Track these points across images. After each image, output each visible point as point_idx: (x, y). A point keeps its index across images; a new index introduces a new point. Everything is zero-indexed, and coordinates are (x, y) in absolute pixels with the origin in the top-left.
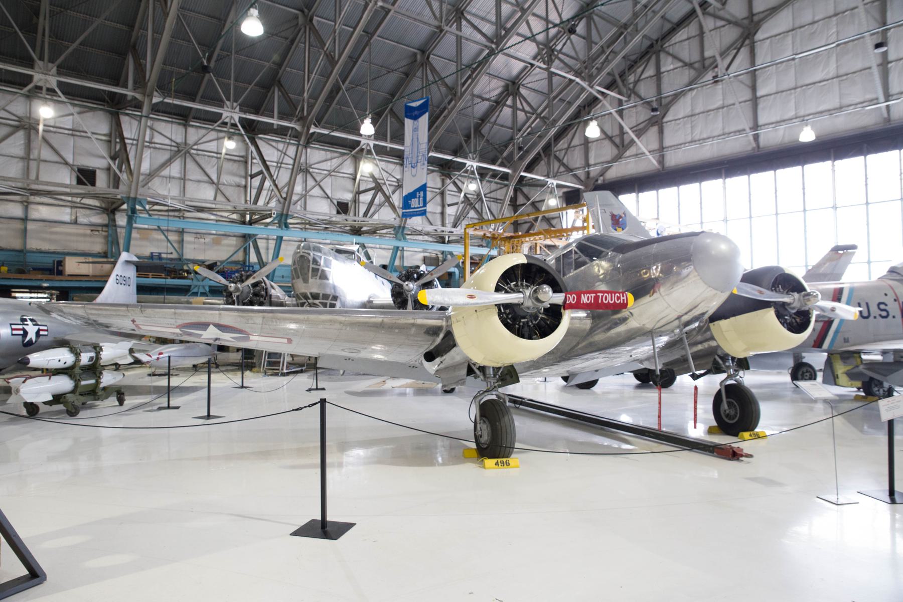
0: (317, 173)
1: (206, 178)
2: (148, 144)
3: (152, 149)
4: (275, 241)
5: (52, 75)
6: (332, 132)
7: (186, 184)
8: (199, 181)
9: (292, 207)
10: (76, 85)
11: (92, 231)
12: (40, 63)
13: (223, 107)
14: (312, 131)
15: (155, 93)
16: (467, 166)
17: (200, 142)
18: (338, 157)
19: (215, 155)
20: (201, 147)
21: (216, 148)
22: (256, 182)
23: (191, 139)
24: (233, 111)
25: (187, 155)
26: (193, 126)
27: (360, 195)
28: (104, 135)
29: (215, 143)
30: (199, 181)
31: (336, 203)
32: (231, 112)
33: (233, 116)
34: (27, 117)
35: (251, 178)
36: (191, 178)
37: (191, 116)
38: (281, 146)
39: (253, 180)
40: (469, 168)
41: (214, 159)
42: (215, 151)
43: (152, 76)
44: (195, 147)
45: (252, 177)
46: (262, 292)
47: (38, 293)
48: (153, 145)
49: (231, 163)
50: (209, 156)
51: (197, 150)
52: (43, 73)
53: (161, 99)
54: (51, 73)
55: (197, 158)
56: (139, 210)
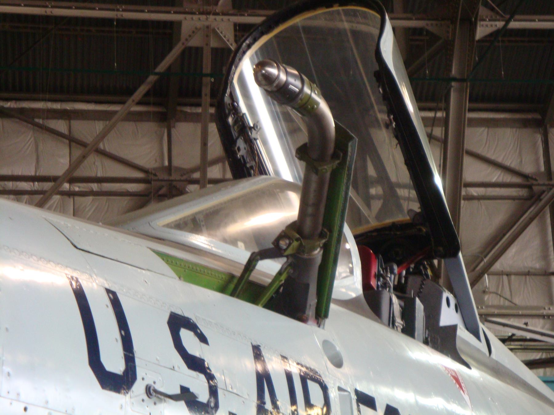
5: (224, 14)
15: (482, 11)
24: (209, 8)
33: (214, 25)
34: (163, 169)
38: (267, 74)
46: (107, 235)
53: (500, 24)
54: (218, 9)
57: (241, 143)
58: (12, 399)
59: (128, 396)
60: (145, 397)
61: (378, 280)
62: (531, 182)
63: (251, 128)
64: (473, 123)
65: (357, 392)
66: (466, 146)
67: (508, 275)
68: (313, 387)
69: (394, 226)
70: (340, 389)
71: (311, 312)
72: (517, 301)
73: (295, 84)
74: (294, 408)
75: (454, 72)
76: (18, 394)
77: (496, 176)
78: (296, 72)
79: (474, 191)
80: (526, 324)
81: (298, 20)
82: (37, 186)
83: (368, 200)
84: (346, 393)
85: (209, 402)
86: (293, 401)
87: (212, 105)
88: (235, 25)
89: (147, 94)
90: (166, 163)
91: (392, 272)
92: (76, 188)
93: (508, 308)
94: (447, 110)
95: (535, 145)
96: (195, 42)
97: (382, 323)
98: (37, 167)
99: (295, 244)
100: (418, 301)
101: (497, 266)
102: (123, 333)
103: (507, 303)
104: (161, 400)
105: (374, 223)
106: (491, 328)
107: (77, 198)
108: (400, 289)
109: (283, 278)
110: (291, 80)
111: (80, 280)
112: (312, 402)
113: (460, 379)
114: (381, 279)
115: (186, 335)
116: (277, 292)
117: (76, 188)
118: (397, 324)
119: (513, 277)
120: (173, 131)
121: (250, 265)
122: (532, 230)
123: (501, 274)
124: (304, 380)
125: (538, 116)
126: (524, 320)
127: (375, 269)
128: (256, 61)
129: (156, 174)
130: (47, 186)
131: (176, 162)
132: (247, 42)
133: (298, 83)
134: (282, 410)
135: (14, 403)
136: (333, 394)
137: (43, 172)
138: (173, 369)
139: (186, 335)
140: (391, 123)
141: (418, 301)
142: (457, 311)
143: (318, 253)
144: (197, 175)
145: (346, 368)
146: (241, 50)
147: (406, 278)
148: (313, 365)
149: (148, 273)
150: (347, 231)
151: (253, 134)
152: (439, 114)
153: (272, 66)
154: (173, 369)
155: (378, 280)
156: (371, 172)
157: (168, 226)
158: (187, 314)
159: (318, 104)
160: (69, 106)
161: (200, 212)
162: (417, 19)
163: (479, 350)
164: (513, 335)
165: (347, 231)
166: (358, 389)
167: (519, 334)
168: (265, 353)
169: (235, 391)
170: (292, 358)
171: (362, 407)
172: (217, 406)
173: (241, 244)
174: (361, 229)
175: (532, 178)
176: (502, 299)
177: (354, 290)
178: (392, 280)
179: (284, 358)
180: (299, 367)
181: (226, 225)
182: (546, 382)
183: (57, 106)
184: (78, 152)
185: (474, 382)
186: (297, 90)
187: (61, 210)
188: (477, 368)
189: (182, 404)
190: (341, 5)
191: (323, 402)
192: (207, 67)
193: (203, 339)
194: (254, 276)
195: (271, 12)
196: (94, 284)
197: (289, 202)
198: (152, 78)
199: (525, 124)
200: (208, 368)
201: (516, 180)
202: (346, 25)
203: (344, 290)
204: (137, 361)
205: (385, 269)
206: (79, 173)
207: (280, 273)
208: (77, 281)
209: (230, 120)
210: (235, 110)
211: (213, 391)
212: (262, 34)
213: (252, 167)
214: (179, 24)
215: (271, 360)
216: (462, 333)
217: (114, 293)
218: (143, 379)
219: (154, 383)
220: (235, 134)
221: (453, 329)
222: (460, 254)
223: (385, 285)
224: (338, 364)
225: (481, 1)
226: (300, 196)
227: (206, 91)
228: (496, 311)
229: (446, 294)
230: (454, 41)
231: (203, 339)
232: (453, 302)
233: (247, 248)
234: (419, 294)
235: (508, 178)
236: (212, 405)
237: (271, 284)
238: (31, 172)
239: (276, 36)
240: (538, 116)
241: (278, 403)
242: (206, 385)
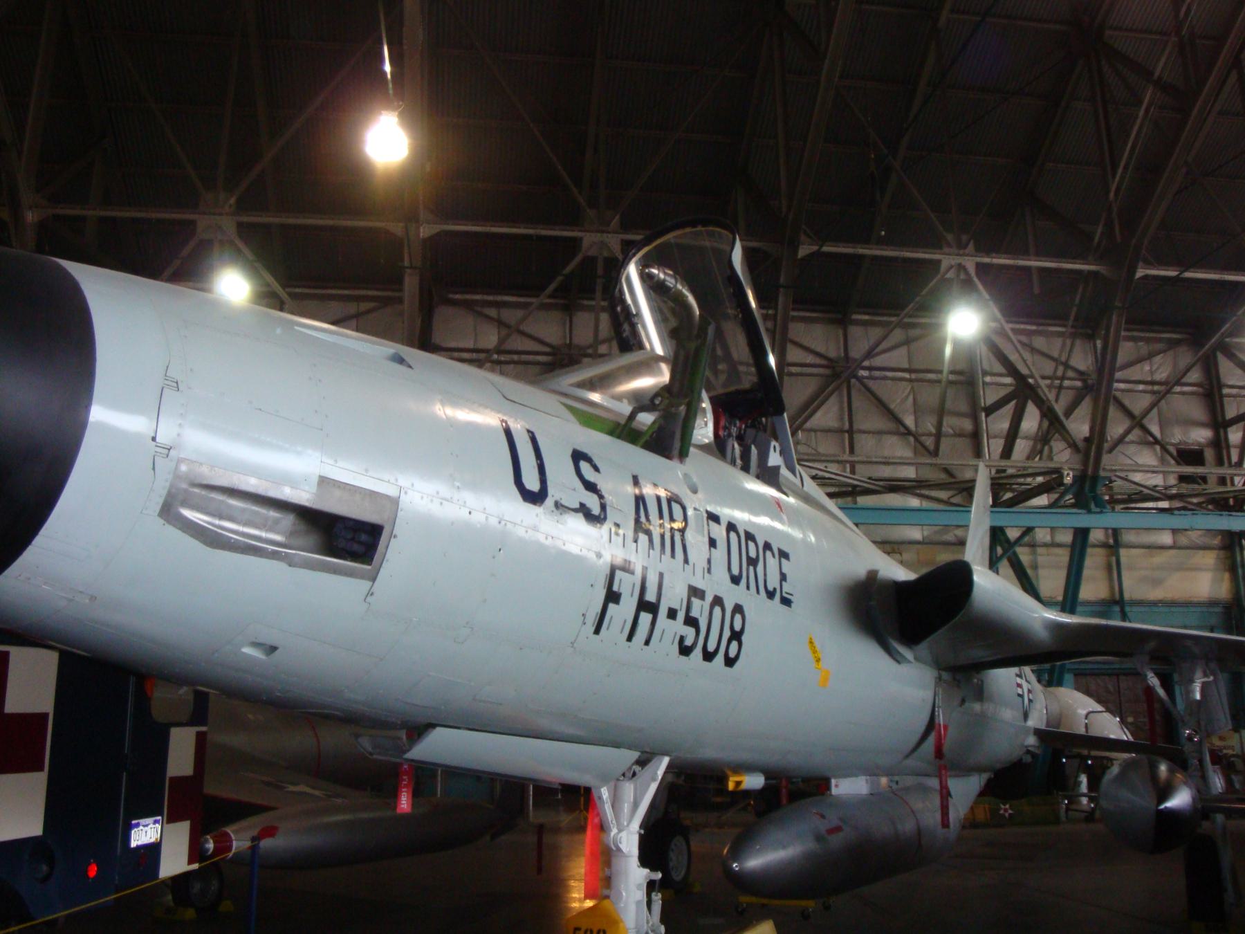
0: (1123, 391)
1: (891, 425)
4: (1069, 549)
6: (1185, 271)
7: (855, 440)
8: (880, 433)
9: (1106, 460)
12: (591, 213)
13: (940, 248)
14: (1140, 273)
15: (803, 237)
17: (878, 350)
18: (1165, 351)
19: (907, 375)
20: (878, 361)
21: (906, 360)
22: (1000, 423)
23: (858, 348)
24: (961, 252)
25: (853, 381)
27: (1229, 430)
29: (903, 351)
30: (880, 433)
31: (1175, 453)
32: (957, 255)
35: (987, 416)
36: (863, 427)
39: (990, 419)
41: (904, 383)
42: (906, 366)
44: (866, 363)
45: (990, 411)
47: (367, 289)
50: (893, 379)
51: (870, 369)
52: (598, 231)
53: (815, 248)
55: (870, 383)
56: (1095, 346)
57: (626, 327)
58: (461, 505)
59: (542, 508)
60: (554, 509)
61: (725, 431)
63: (634, 315)
64: (795, 319)
65: (707, 512)
66: (789, 336)
67: (815, 431)
68: (675, 507)
69: (738, 392)
70: (695, 509)
71: (676, 452)
72: (821, 450)
73: (670, 282)
74: (662, 521)
75: (782, 280)
76: (465, 502)
77: (810, 359)
78: (671, 272)
79: (794, 369)
80: (826, 467)
81: (669, 237)
82: (474, 356)
83: (716, 372)
84: (699, 512)
85: (600, 515)
86: (661, 517)
87: (604, 300)
88: (622, 240)
89: (556, 290)
90: (568, 342)
91: (735, 426)
92: (502, 358)
93: (813, 455)
94: (776, 308)
96: (591, 253)
97: (726, 462)
98: (476, 341)
99: (666, 402)
100: (753, 447)
101: (808, 425)
102: (539, 462)
103: (813, 452)
104: (565, 512)
105: (721, 391)
106: (515, 524)
107: (502, 366)
108: (740, 438)
109: (656, 426)
110: (668, 278)
111: (509, 423)
112: (675, 517)
113: (781, 504)
114: (727, 430)
115: (584, 466)
116: (651, 436)
117: (502, 358)
118: (737, 464)
119: (819, 433)
120: (575, 320)
121: (632, 416)
122: (833, 400)
123: (810, 430)
124: (669, 501)
125: (840, 316)
126: (825, 464)
127: (723, 423)
128: (643, 264)
130: (482, 356)
131: (576, 341)
132: (633, 251)
133: (673, 281)
134: (653, 522)
135: (462, 507)
136: (690, 512)
137: (481, 345)
138: (574, 490)
139: (584, 466)
140: (738, 315)
141: (753, 447)
142: (781, 455)
143: (682, 408)
144: (590, 351)
145: (700, 495)
146: (629, 257)
147: (745, 430)
148: (676, 491)
149: (557, 419)
150: (704, 395)
151: (635, 320)
152: (770, 312)
153: (653, 268)
154: (574, 490)
155: (725, 431)
156: (719, 352)
157: (572, 385)
158: (585, 450)
159: (687, 297)
160: (499, 298)
161: (595, 376)
163: (795, 484)
164: (817, 475)
165: (704, 395)
166: (709, 509)
167: (821, 474)
168: (641, 481)
169: (619, 508)
170: (1082, 389)
171: (711, 522)
172: (605, 519)
173: (625, 401)
174: (713, 393)
176: (810, 449)
177: (707, 437)
178: (734, 431)
179: (655, 485)
180: (666, 492)
181: (615, 386)
182: (840, 508)
183: (490, 298)
184: (504, 332)
185: (790, 506)
186: (672, 286)
187: (493, 370)
188: (794, 497)
189: (580, 515)
190: (703, 226)
191: (682, 518)
192: (600, 271)
193: (596, 469)
194: (634, 425)
195: (648, 232)
196: (519, 426)
197: (660, 373)
198: (560, 278)
199: (832, 322)
200: (600, 490)
201: (823, 362)
202: (707, 244)
203: (700, 437)
204: (549, 483)
205: (730, 424)
206: (503, 348)
207: (654, 422)
208: (506, 422)
209: (619, 309)
210: (623, 301)
211: (603, 507)
212: (645, 245)
213: (634, 345)
214: (581, 239)
215: (646, 486)
216: (784, 472)
217: (532, 433)
218: (553, 496)
219: (561, 499)
220: (622, 319)
221: (777, 468)
222: (785, 415)
223: (730, 435)
224: (695, 491)
226: (670, 367)
227: (599, 288)
228: (806, 457)
229: (773, 443)
231: (596, 469)
232: (778, 449)
233: (630, 403)
234: (754, 442)
235: (818, 361)
236: (602, 517)
237: (647, 430)
238: (471, 346)
239: (655, 247)
241: (650, 518)
242: (599, 503)
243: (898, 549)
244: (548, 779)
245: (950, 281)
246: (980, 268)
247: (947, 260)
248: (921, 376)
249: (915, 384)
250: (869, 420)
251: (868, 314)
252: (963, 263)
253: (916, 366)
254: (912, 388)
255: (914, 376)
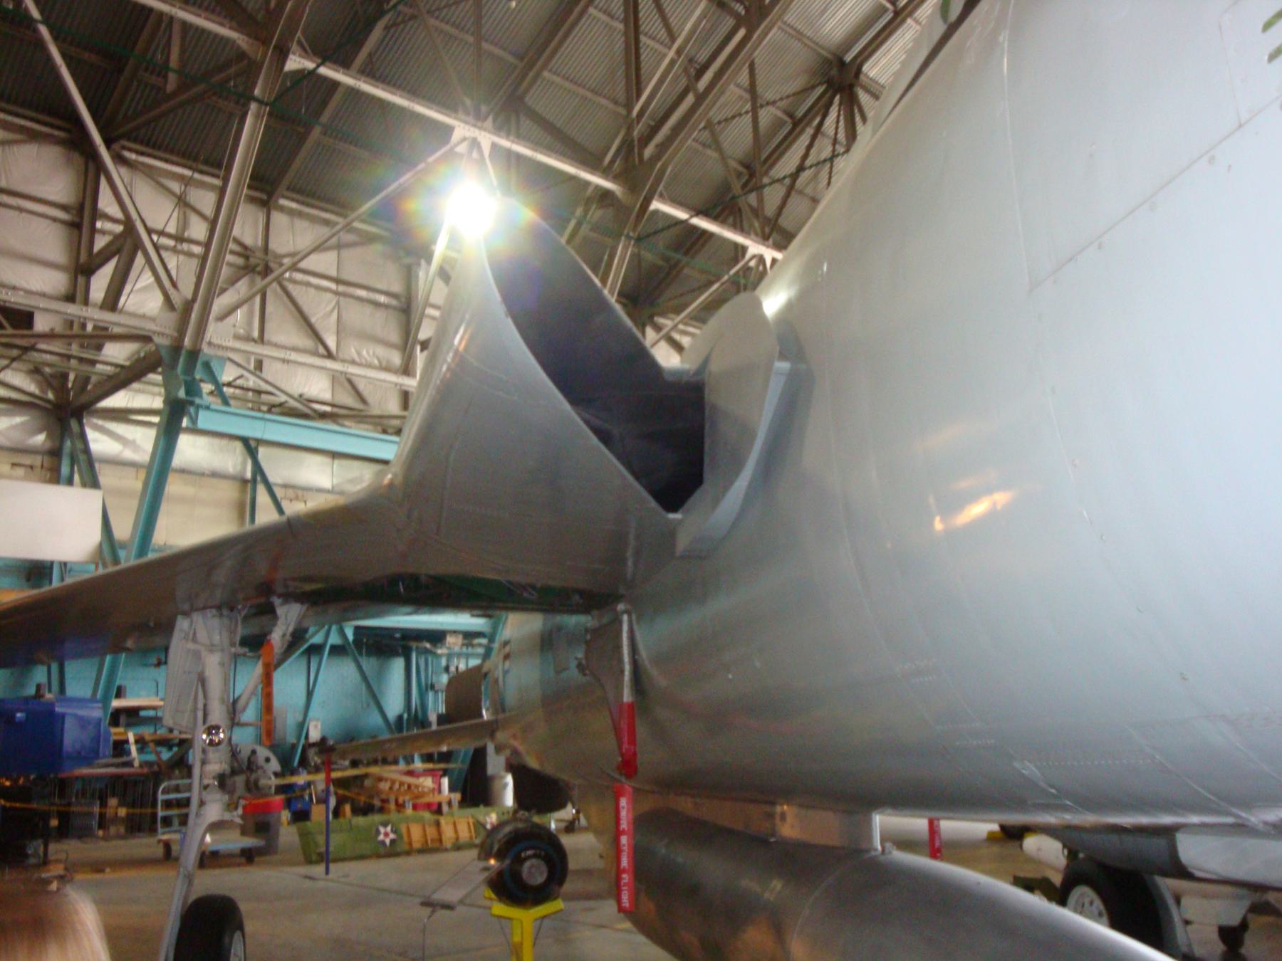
2: (171, 243)
3: (182, 257)
10: (73, 75)
11: (14, 465)
15: (295, 47)
16: (748, 256)
19: (333, 286)
26: (282, 209)
28: (64, 208)
37: (285, 183)
40: (752, 264)
41: (329, 295)
42: (333, 273)
43: (801, 152)
48: (185, 246)
49: (368, 309)
50: (318, 288)
55: (290, 287)
62: (249, 253)
75: (257, 92)
95: (256, 222)
125: (264, 197)
129: (623, 19)
162: (231, 28)
175: (250, 250)
225: (1012, 2)
230: (263, 63)
240: (264, 197)
243: (303, 496)
244: (105, 946)
245: (461, 156)
246: (494, 146)
247: (462, 130)
248: (351, 290)
249: (342, 299)
250: (284, 331)
251: (297, 201)
252: (479, 139)
253: (345, 277)
254: (338, 303)
255: (341, 288)
